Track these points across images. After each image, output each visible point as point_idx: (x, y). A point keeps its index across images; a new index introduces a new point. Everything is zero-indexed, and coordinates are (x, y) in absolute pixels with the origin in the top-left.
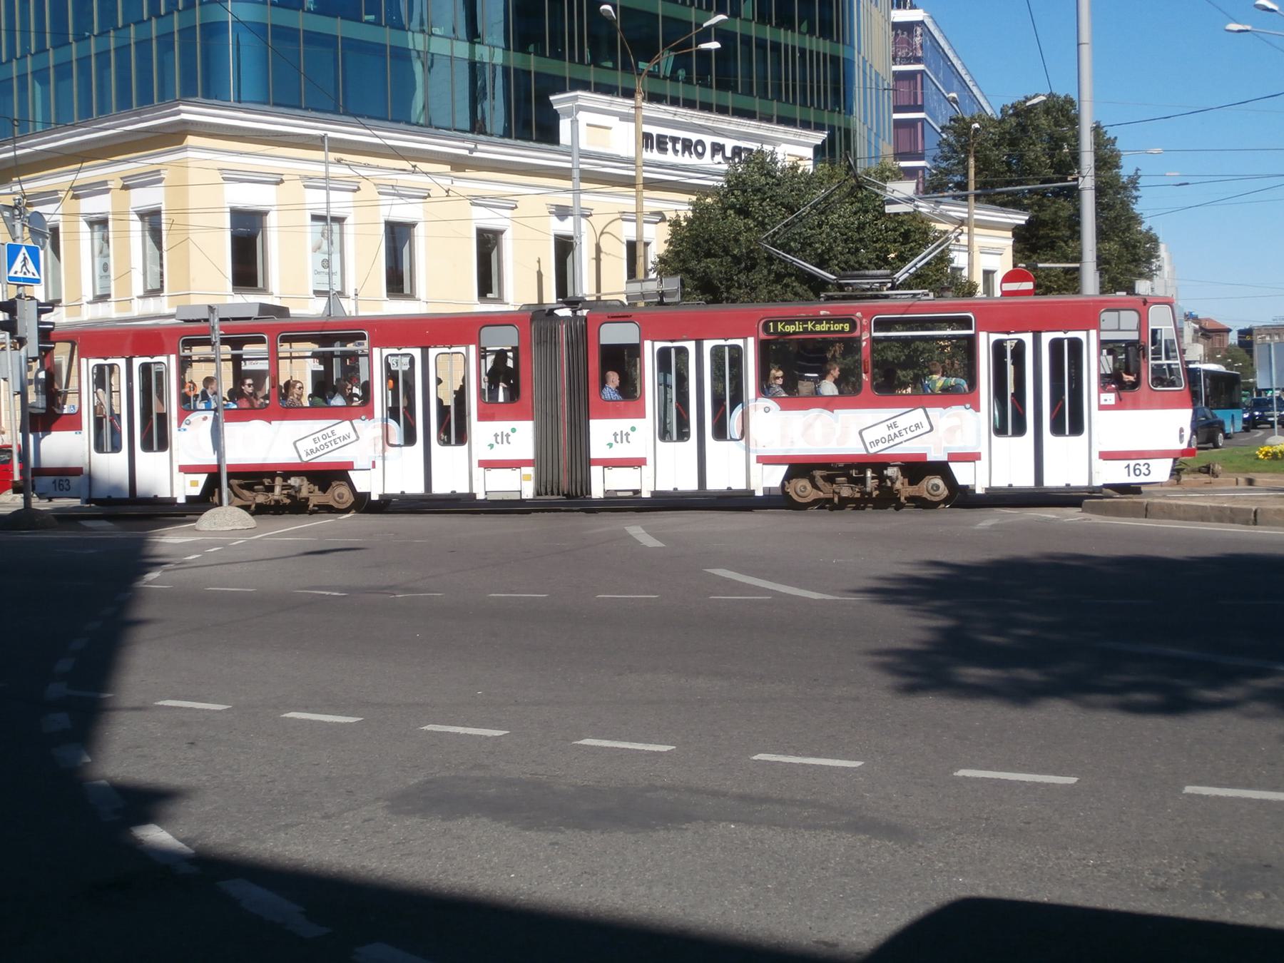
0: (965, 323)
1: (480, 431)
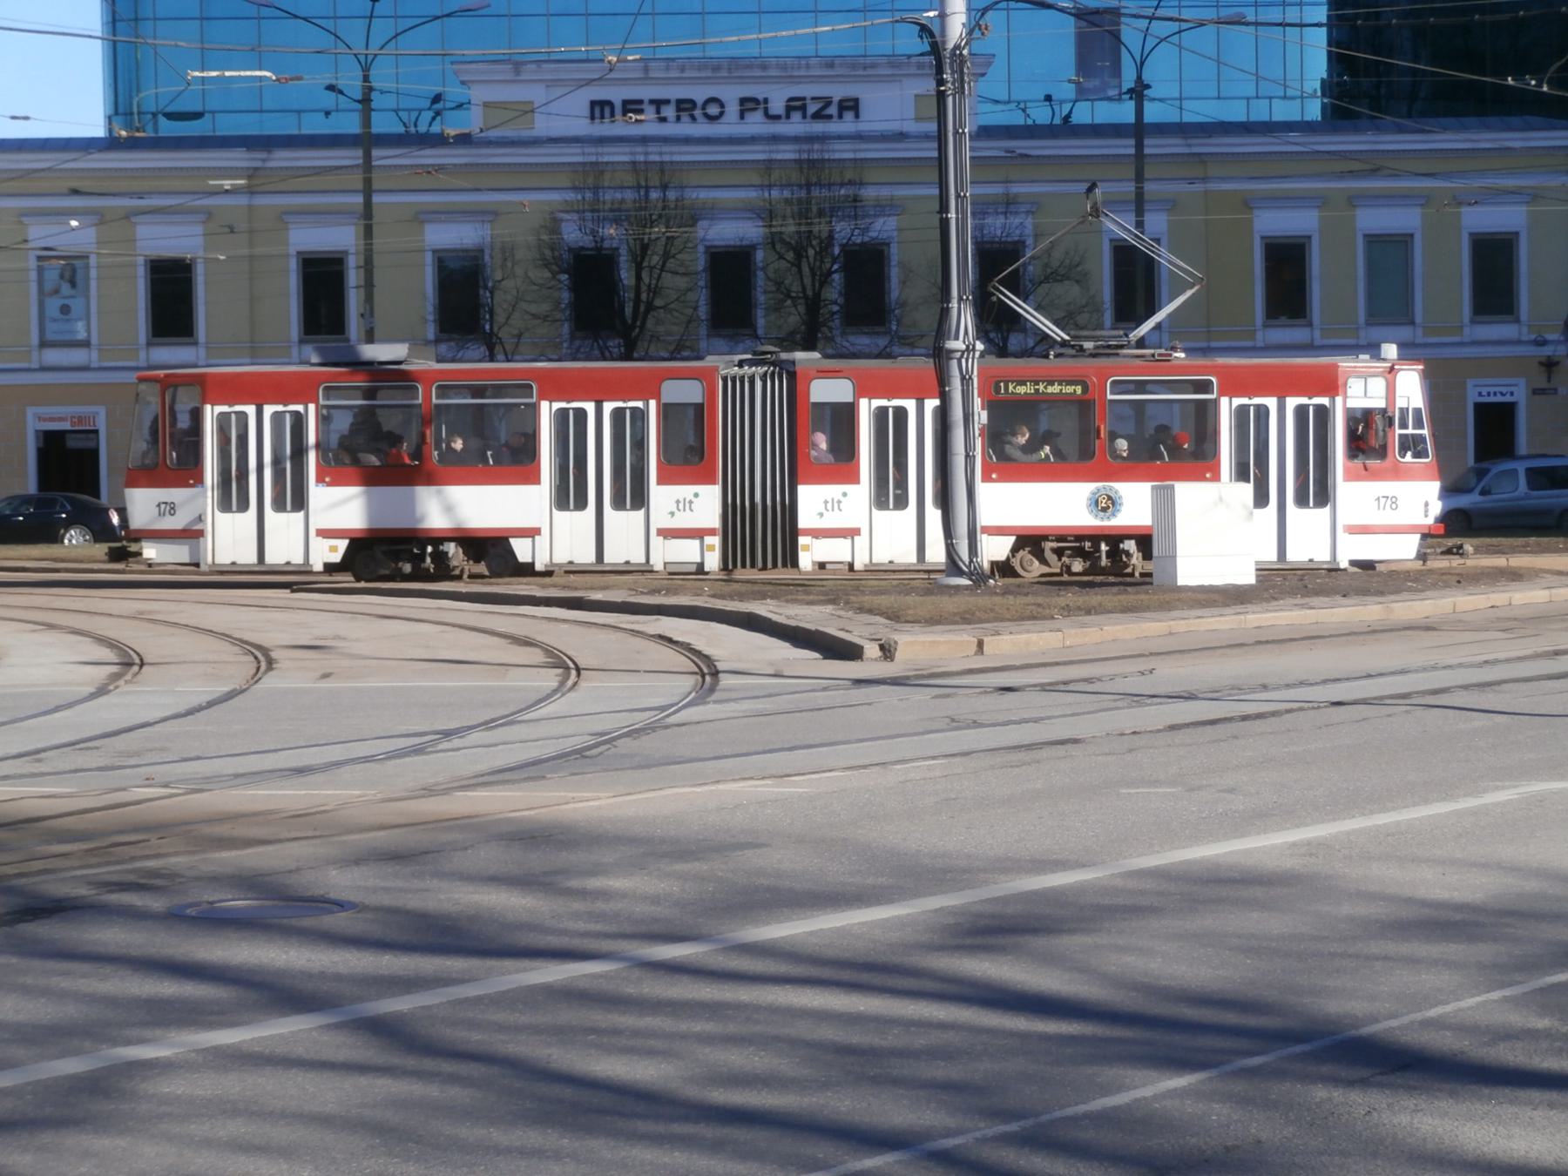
0: (1204, 387)
1: (662, 496)
